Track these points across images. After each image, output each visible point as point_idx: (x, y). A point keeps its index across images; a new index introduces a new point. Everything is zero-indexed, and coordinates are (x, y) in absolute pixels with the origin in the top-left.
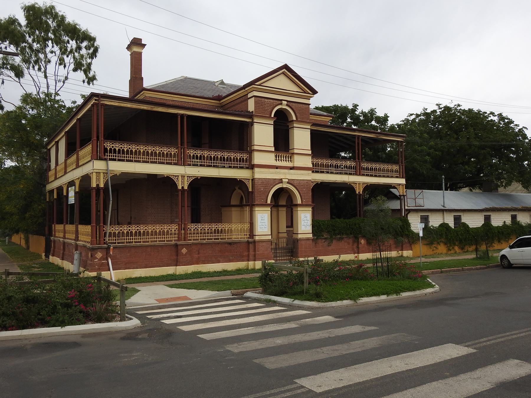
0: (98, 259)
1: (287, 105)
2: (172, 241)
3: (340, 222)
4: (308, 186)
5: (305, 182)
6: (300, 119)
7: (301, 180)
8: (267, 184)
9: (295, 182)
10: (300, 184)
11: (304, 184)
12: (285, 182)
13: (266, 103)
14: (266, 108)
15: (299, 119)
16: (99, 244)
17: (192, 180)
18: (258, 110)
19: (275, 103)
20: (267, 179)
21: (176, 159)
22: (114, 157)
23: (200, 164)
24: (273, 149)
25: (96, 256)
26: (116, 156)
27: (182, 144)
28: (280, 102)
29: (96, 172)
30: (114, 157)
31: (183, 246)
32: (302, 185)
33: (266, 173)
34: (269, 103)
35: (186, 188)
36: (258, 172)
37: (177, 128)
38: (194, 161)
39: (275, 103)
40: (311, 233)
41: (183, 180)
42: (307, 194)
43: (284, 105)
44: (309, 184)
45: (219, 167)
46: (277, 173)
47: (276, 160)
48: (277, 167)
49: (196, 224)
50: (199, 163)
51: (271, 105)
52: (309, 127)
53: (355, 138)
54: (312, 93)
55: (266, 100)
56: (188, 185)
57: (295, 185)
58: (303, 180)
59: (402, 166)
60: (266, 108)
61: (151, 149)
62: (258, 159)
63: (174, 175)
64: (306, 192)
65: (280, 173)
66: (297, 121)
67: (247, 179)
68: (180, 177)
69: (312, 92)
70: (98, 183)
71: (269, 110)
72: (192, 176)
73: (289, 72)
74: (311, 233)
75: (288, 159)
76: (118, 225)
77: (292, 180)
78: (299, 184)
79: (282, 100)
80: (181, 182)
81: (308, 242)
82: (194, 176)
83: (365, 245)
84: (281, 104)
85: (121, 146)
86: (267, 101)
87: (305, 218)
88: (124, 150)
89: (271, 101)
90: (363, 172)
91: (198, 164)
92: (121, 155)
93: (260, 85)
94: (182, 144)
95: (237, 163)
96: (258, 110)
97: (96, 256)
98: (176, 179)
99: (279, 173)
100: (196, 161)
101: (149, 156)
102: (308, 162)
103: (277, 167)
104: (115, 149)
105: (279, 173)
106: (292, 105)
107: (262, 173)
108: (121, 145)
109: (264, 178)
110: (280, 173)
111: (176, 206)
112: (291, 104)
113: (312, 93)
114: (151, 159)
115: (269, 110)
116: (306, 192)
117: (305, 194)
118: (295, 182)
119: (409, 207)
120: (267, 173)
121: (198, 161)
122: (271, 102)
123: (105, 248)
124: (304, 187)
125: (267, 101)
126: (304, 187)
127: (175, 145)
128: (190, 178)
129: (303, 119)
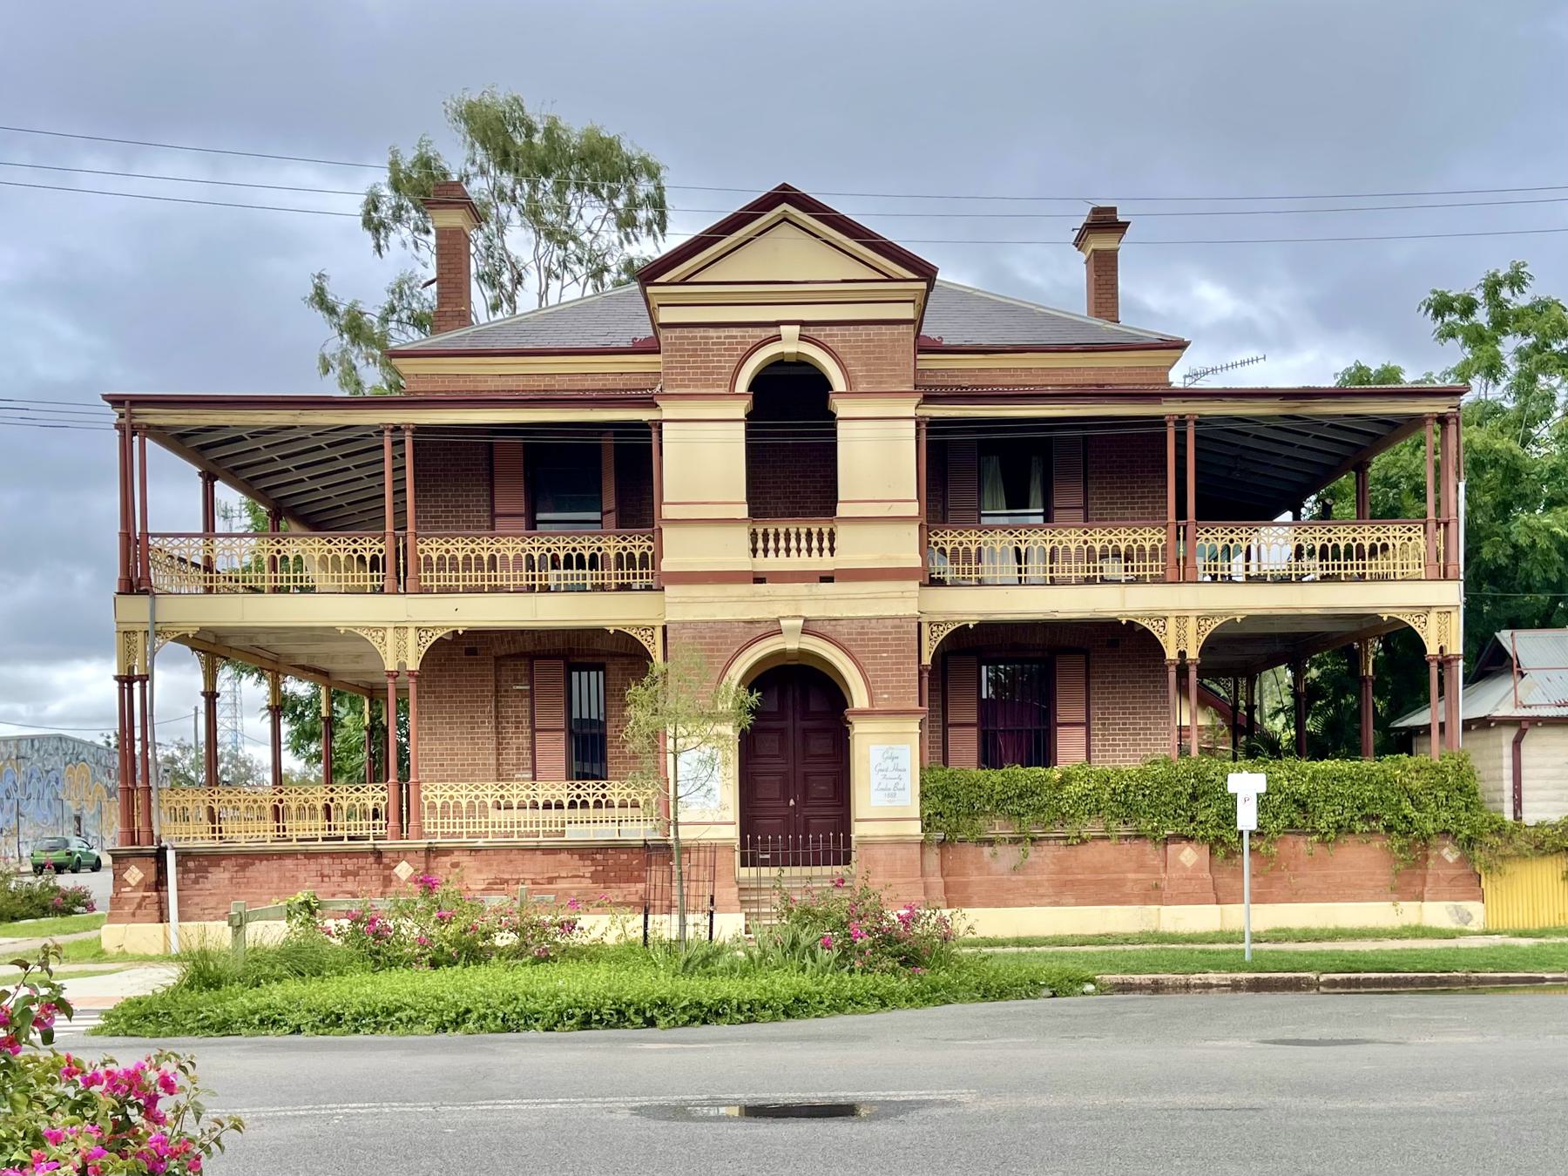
0: (130, 886)
1: (802, 338)
2: (512, 837)
3: (590, 789)
4: (903, 639)
5: (887, 627)
6: (868, 383)
7: (869, 619)
8: (720, 641)
9: (843, 628)
10: (867, 633)
11: (881, 633)
12: (792, 630)
13: (713, 344)
14: (713, 361)
15: (862, 387)
16: (139, 844)
17: (946, 633)
18: (677, 374)
19: (750, 337)
20: (715, 622)
21: (1160, 563)
22: (282, 581)
23: (540, 585)
24: (742, 511)
25: (125, 876)
26: (457, 579)
27: (401, 526)
28: (772, 332)
29: (125, 632)
30: (282, 581)
31: (402, 854)
32: (873, 639)
33: (711, 599)
34: (724, 344)
35: (1193, 654)
36: (678, 600)
37: (1197, 461)
38: (572, 575)
39: (750, 337)
40: (916, 819)
41: (1182, 632)
42: (899, 669)
43: (790, 341)
44: (905, 633)
45: (1392, 578)
46: (759, 599)
47: (754, 551)
48: (759, 579)
49: (577, 783)
50: (486, 583)
51: (736, 349)
52: (908, 408)
53: (1165, 424)
54: (916, 277)
55: (712, 332)
56: (933, 651)
57: (841, 639)
58: (879, 618)
59: (405, 538)
60: (713, 361)
61: (463, 549)
62: (678, 551)
63: (369, 628)
64: (894, 664)
65: (771, 598)
66: (851, 393)
67: (377, 630)
68: (390, 634)
69: (915, 274)
70: (1182, 648)
71: (724, 367)
72: (434, 628)
73: (805, 211)
74: (916, 819)
75: (799, 544)
76: (375, 782)
77: (826, 623)
78: (859, 634)
79: (777, 324)
80: (409, 654)
81: (901, 852)
82: (443, 628)
83: (1202, 870)
84: (778, 338)
85: (961, 538)
86: (715, 335)
87: (890, 765)
88: (556, 555)
89: (734, 332)
90: (429, 578)
91: (458, 586)
92: (1060, 565)
93: (683, 283)
94: (1181, 513)
95: (631, 571)
96: (677, 374)
97: (125, 876)
98: (380, 640)
99: (768, 598)
100: (578, 575)
101: (1070, 563)
102: (732, 550)
103: (759, 579)
104: (1239, 545)
105: (768, 598)
106: (831, 335)
107: (694, 601)
108: (961, 534)
109: (702, 622)
110: (771, 598)
111: (517, 728)
112: (812, 332)
113: (916, 277)
114: (515, 580)
115: (724, 367)
116: (894, 664)
117: (892, 670)
118: (839, 628)
119: (1530, 707)
120: (716, 600)
121: (1297, 570)
122: (735, 337)
123: (151, 855)
124: (881, 645)
125: (715, 335)
126: (881, 645)
127: (1154, 515)
128: (1209, 622)
129: (881, 383)
